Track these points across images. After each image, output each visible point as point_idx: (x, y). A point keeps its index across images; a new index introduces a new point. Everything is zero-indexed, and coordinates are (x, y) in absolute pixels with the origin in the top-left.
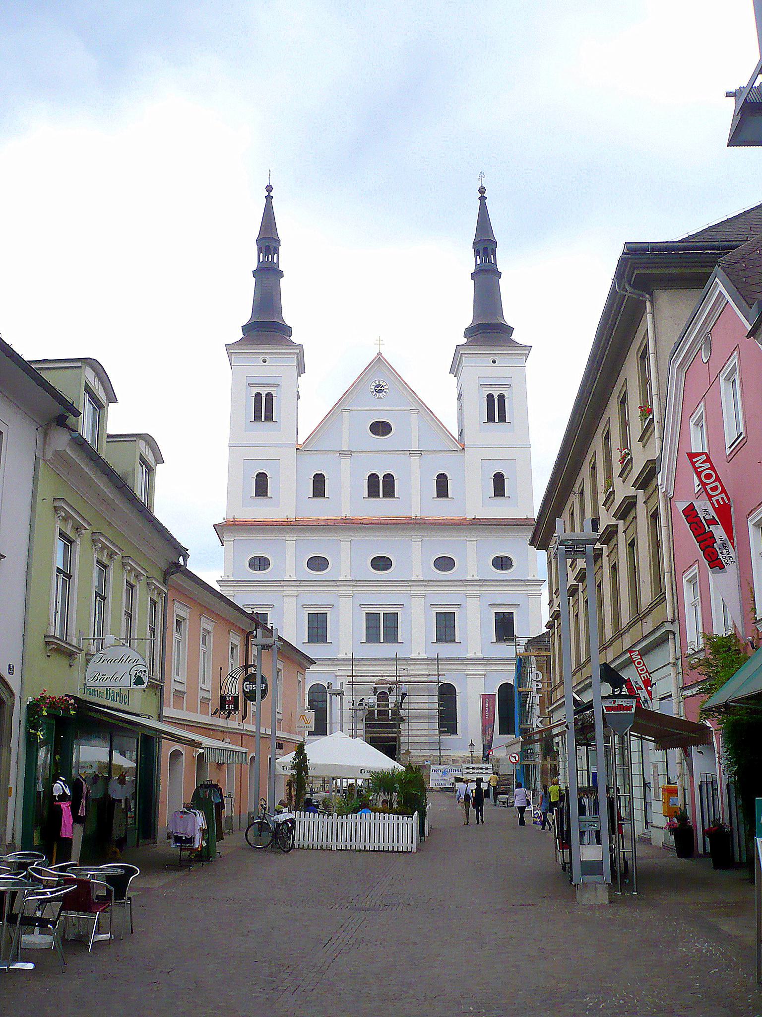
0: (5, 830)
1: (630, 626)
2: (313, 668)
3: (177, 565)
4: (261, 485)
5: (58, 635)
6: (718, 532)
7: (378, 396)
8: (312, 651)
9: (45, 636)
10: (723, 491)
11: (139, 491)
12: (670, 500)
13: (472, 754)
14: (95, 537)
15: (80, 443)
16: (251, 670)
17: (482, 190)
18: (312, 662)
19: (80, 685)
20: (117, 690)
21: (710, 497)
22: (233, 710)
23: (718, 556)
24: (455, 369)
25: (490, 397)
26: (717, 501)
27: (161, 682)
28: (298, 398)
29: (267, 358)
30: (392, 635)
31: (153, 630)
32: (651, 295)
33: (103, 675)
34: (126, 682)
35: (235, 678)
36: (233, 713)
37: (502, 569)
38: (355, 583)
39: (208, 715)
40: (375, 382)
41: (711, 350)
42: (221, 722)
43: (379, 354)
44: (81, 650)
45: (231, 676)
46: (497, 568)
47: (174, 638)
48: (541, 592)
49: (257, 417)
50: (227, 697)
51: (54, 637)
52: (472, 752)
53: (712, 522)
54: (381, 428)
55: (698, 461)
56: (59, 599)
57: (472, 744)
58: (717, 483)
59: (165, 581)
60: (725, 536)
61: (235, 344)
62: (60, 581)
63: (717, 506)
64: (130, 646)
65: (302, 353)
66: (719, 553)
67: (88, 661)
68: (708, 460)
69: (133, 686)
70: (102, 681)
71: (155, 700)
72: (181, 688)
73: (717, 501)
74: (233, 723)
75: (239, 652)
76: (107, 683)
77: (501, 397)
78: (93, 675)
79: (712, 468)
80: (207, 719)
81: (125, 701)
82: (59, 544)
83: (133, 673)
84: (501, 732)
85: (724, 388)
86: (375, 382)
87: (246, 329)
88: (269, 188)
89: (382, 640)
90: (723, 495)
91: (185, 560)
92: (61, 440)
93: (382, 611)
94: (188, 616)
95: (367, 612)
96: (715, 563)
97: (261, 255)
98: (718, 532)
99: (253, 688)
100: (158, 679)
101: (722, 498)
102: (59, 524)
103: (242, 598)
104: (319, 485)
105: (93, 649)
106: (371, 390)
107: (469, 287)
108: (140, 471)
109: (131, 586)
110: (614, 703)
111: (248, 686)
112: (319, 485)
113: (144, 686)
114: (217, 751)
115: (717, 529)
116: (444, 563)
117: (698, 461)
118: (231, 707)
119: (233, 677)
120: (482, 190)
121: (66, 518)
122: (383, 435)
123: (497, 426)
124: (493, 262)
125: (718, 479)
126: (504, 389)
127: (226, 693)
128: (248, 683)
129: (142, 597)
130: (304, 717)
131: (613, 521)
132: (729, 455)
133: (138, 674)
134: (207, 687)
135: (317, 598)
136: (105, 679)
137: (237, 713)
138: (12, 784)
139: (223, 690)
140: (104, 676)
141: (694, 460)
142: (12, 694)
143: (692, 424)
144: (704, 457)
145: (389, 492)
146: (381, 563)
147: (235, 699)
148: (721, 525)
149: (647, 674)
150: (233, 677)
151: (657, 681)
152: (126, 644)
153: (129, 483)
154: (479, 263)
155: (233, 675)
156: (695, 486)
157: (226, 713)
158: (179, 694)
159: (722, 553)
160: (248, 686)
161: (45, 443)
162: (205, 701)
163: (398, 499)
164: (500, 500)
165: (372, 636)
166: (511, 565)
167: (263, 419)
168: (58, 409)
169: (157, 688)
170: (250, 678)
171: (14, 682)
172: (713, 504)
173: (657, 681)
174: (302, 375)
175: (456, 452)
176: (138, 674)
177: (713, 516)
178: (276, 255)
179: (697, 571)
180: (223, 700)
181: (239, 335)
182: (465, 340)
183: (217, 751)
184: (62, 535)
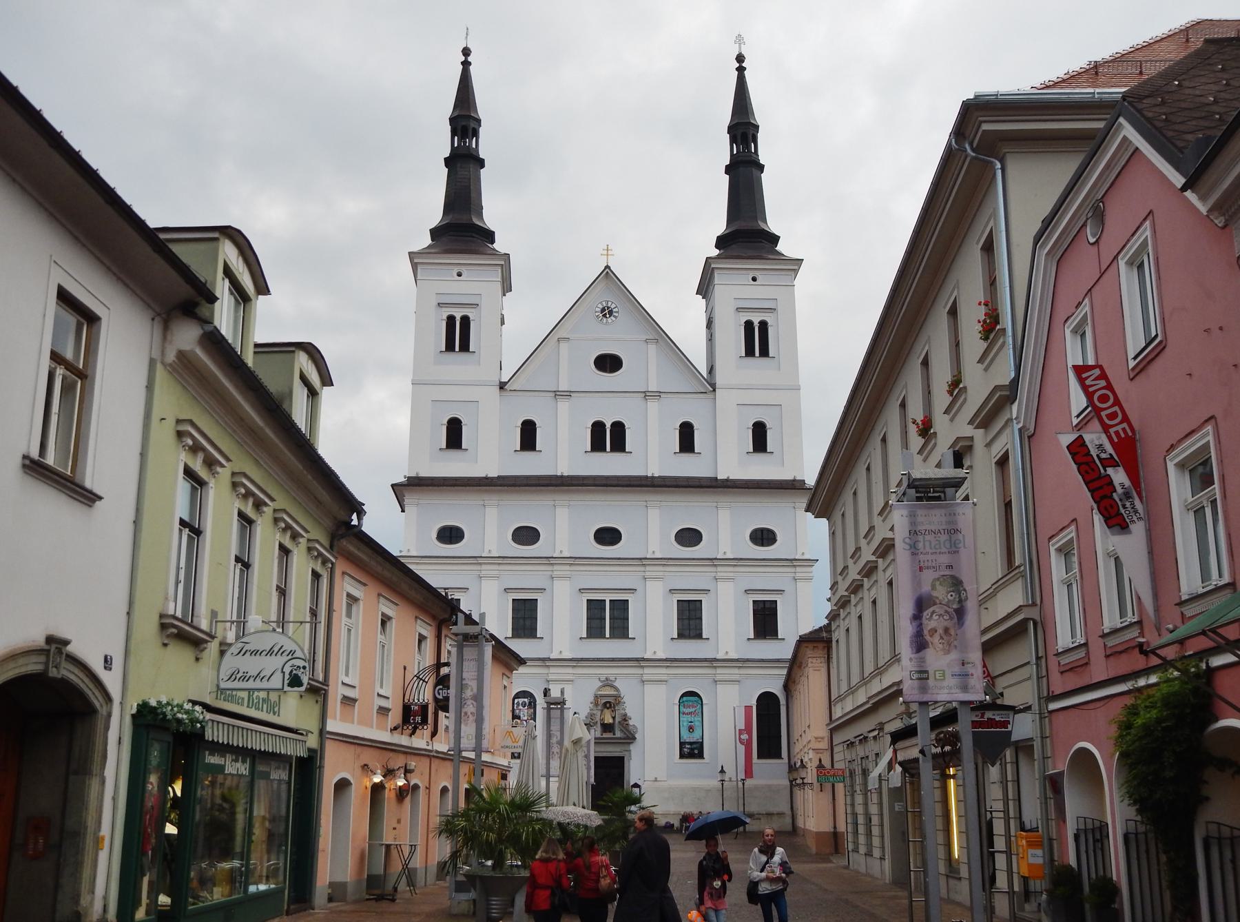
0: (93, 899)
2: (522, 670)
3: (348, 524)
4: (454, 434)
5: (179, 614)
6: (1119, 477)
7: (605, 321)
8: (521, 647)
9: (162, 616)
10: (1125, 419)
11: (300, 418)
12: (1029, 441)
13: (722, 784)
14: (237, 479)
15: (214, 341)
16: (444, 671)
17: (740, 58)
18: (522, 661)
19: (210, 687)
20: (263, 695)
21: (1106, 429)
22: (420, 724)
23: (1119, 510)
24: (705, 288)
25: (749, 325)
26: (1117, 433)
27: (323, 684)
28: (503, 323)
30: (621, 630)
31: (314, 613)
32: (1002, 161)
33: (244, 673)
34: (276, 682)
35: (424, 681)
36: (420, 727)
38: (574, 560)
39: (387, 731)
40: (601, 303)
41: (1103, 225)
42: (403, 740)
43: (607, 267)
44: (213, 637)
45: (418, 677)
47: (343, 626)
48: (811, 575)
49: (450, 347)
50: (412, 707)
51: (174, 617)
52: (722, 781)
53: (1109, 462)
54: (608, 363)
55: (1089, 376)
56: (183, 564)
57: (722, 771)
58: (1116, 408)
59: (332, 546)
60: (1127, 483)
61: (420, 253)
62: (185, 538)
63: (1116, 440)
64: (283, 632)
66: (1120, 507)
67: (222, 653)
68: (1103, 376)
69: (286, 688)
70: (243, 680)
71: (316, 710)
72: (350, 693)
73: (1117, 433)
74: (420, 741)
75: (429, 645)
76: (250, 684)
77: (764, 325)
78: (229, 673)
79: (1109, 387)
80: (385, 736)
81: (274, 710)
82: (183, 488)
83: (287, 670)
84: (759, 757)
85: (1127, 279)
86: (601, 303)
87: (436, 233)
88: (466, 52)
89: (608, 635)
90: (1125, 425)
91: (359, 519)
92: (187, 336)
93: (608, 597)
94: (362, 594)
95: (588, 598)
96: (1116, 521)
97: (456, 138)
98: (1119, 477)
100: (321, 680)
101: (1124, 430)
102: (184, 457)
103: (436, 577)
105: (231, 636)
107: (723, 182)
108: (300, 395)
109: (284, 551)
110: (982, 717)
111: (440, 691)
113: (303, 689)
114: (245, 734)
115: (1117, 472)
116: (689, 537)
117: (1089, 376)
118: (418, 719)
119: (421, 679)
120: (740, 58)
121: (195, 449)
123: (757, 362)
124: (753, 151)
125: (1117, 402)
126: (767, 314)
127: (411, 701)
128: (441, 687)
129: (301, 565)
130: (511, 734)
132: (1133, 369)
133: (294, 672)
134: (389, 691)
135: (526, 579)
136: (247, 678)
137: (425, 727)
138: (105, 831)
140: (245, 674)
141: (1084, 376)
142: (108, 698)
143: (1068, 332)
144: (1097, 372)
145: (619, 444)
146: (608, 536)
147: (424, 708)
148: (1121, 467)
149: (989, 678)
150: (421, 679)
151: (1004, 688)
152: (278, 630)
153: (285, 406)
154: (735, 152)
155: (421, 677)
156: (1073, 417)
157: (410, 727)
158: (348, 701)
159: (1124, 507)
160: (440, 691)
161: (164, 338)
162: (383, 711)
164: (760, 456)
165: (595, 630)
167: (457, 348)
168: (185, 290)
169: (318, 692)
170: (443, 681)
171: (112, 681)
172: (1110, 438)
173: (1004, 688)
174: (507, 294)
175: (705, 395)
176: (294, 672)
177: (1110, 454)
178: (475, 138)
179: (1073, 534)
180: (407, 710)
182: (717, 252)
183: (245, 734)
184: (189, 473)
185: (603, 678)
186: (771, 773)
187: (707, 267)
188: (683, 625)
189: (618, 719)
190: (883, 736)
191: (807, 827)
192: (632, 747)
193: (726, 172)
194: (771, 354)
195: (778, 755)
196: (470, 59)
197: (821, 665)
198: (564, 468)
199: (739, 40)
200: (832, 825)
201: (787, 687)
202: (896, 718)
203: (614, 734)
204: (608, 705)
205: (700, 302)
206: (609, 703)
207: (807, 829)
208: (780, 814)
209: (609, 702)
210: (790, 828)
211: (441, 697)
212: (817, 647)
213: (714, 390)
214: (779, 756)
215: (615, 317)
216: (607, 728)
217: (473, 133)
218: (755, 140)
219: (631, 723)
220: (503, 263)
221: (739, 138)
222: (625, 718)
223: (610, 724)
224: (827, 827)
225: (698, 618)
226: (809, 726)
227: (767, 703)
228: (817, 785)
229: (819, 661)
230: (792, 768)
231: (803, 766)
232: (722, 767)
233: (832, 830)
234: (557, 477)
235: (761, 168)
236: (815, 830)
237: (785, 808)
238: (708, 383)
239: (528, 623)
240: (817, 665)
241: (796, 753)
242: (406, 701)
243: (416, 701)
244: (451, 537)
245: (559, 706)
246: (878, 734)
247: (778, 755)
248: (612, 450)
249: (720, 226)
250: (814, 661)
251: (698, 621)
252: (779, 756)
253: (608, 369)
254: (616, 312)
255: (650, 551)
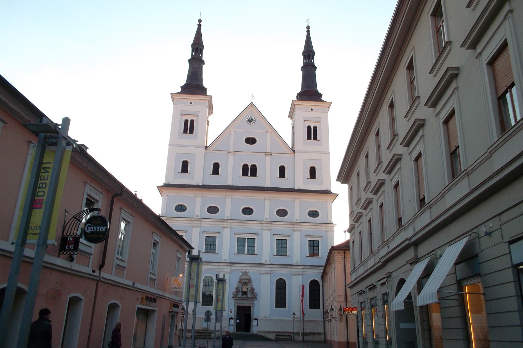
1: (380, 248)
17: (308, 27)
22: (72, 250)
24: (291, 116)
25: (309, 128)
28: (208, 125)
29: (192, 101)
37: (313, 217)
40: (249, 117)
46: (310, 217)
50: (69, 238)
52: (294, 318)
54: (251, 141)
57: (294, 314)
65: (211, 100)
87: (182, 88)
88: (200, 21)
93: (247, 237)
99: (94, 229)
104: (216, 169)
106: (247, 121)
111: (89, 228)
112: (216, 169)
118: (72, 247)
120: (308, 27)
122: (251, 144)
123: (312, 141)
127: (68, 234)
128: (89, 224)
131: (361, 211)
137: (76, 253)
139: (66, 231)
160: (89, 228)
163: (258, 178)
165: (240, 251)
166: (318, 215)
181: (180, 90)
185: (243, 271)
186: (316, 314)
187: (293, 104)
188: (278, 250)
189: (249, 289)
190: (391, 281)
191: (333, 339)
192: (255, 302)
193: (301, 70)
194: (318, 139)
195: (318, 308)
196: (201, 24)
197: (341, 261)
198: (230, 182)
199: (308, 20)
200: (346, 338)
201: (323, 277)
202: (407, 264)
203: (247, 296)
204: (245, 283)
205: (290, 121)
206: (245, 282)
207: (332, 341)
208: (319, 334)
209: (246, 282)
210: (323, 340)
211: (88, 232)
212: (339, 252)
213: (294, 153)
214: (319, 308)
215: (254, 123)
216: (245, 293)
217: (200, 51)
218: (313, 58)
219: (255, 291)
220: (209, 99)
221: (307, 57)
222: (252, 289)
223: (246, 292)
224: (343, 339)
225: (285, 252)
226: (332, 294)
227: (314, 285)
228: (339, 317)
229: (340, 259)
230: (325, 313)
231: (332, 309)
232: (294, 312)
233: (346, 341)
234: (227, 186)
235: (315, 68)
236: (338, 341)
237: (321, 331)
238: (292, 150)
239: (212, 247)
240: (339, 261)
241: (326, 306)
242: (65, 234)
243: (72, 234)
244: (181, 210)
245: (222, 282)
246: (387, 280)
247: (318, 308)
248: (251, 175)
249: (299, 89)
250: (338, 259)
251: (285, 248)
252: (319, 308)
253: (250, 143)
254: (254, 121)
255: (265, 218)
